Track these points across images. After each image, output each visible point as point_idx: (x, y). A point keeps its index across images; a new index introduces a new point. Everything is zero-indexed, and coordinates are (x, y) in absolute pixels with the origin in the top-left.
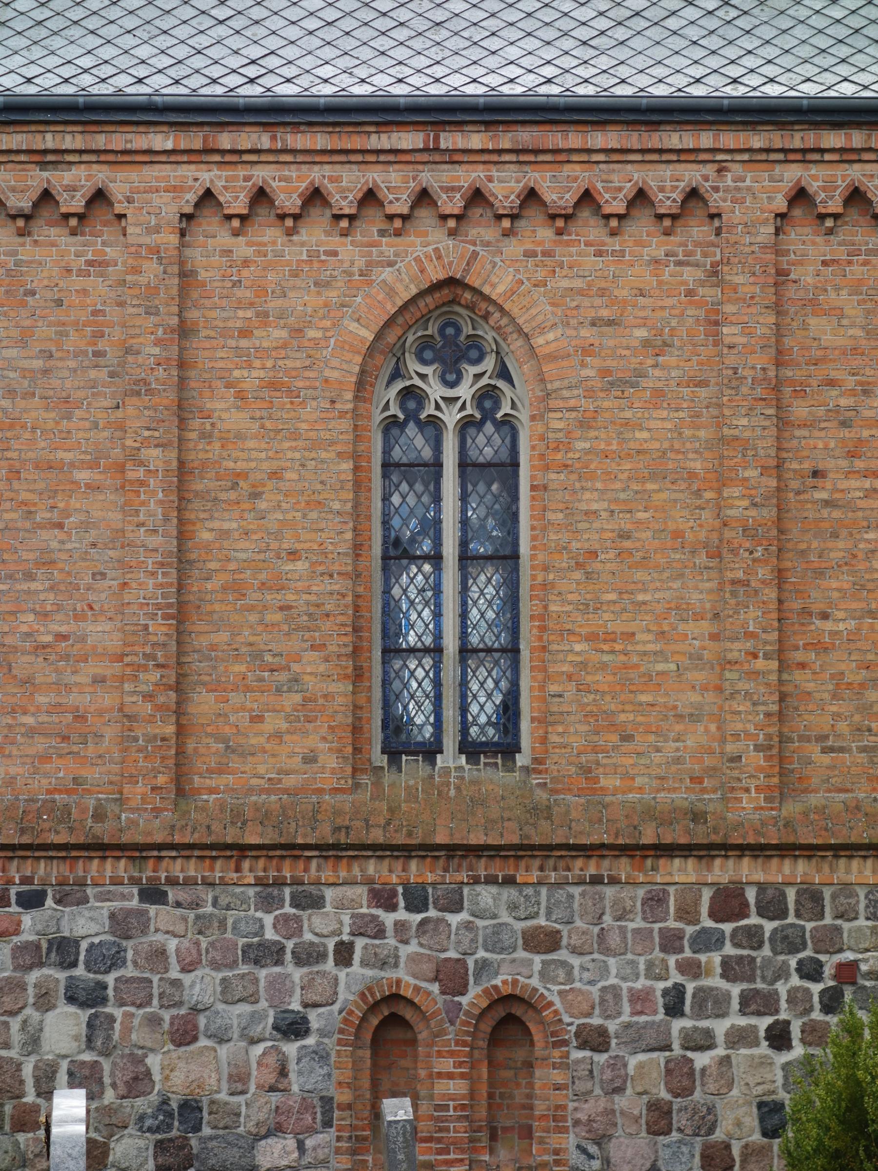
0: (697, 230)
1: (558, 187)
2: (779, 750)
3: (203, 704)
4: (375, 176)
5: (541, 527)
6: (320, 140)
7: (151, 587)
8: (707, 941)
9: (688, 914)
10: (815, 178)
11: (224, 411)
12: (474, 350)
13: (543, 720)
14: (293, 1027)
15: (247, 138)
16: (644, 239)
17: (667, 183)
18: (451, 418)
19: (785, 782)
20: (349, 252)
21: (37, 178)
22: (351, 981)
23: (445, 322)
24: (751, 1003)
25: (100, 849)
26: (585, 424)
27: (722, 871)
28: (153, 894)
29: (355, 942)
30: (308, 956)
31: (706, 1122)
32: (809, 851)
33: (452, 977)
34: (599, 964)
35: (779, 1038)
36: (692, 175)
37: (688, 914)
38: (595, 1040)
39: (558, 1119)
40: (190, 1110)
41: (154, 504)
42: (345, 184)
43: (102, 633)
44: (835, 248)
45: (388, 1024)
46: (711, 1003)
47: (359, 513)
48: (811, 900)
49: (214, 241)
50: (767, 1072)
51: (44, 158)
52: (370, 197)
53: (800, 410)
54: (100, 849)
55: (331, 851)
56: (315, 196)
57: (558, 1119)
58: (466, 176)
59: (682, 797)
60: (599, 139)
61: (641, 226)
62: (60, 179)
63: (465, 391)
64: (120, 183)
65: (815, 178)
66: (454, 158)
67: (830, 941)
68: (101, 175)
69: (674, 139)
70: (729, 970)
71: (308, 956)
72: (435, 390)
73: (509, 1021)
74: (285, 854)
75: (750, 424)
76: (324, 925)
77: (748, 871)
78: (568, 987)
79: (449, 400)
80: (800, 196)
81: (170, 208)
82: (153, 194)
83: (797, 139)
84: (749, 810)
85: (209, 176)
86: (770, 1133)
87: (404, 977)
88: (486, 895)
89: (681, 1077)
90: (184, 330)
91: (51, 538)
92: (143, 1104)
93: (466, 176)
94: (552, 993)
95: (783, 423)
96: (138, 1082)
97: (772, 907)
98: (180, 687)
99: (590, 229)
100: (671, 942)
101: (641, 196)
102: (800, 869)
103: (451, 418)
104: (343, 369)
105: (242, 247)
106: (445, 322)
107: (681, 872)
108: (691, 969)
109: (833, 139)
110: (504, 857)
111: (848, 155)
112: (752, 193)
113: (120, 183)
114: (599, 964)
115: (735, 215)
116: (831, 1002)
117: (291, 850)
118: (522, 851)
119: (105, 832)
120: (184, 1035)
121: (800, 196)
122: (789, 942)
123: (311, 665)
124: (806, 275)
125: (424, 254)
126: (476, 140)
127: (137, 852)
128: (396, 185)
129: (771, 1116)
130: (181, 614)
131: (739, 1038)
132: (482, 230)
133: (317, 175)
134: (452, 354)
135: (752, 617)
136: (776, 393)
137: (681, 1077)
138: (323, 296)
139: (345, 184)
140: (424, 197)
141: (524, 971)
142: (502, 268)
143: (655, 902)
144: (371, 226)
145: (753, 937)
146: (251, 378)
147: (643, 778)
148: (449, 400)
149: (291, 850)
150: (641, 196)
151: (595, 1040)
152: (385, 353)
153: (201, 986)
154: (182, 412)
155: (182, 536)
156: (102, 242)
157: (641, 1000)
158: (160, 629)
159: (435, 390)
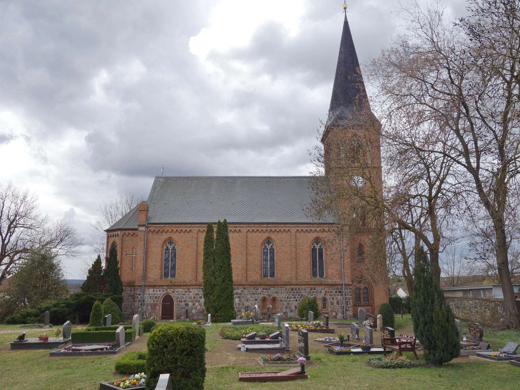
0: (289, 233)
1: (278, 229)
2: (296, 276)
3: (248, 272)
4: (263, 228)
5: (276, 258)
6: (258, 226)
7: (244, 263)
8: (290, 293)
9: (289, 290)
10: (299, 229)
11: (250, 248)
12: (271, 243)
13: (277, 274)
14: (256, 300)
15: (252, 225)
16: (285, 234)
17: (287, 229)
18: (170, 249)
19: (297, 279)
20: (260, 235)
21: (235, 229)
22: (261, 296)
23: (268, 241)
24: (294, 298)
25: (240, 285)
26: (280, 249)
27: (292, 287)
28: (245, 289)
29: (262, 293)
30: (257, 294)
31: (290, 308)
32: (299, 285)
33: (269, 296)
34: (282, 295)
35: (296, 301)
36: (289, 228)
37: (289, 290)
38: (281, 301)
39: (278, 308)
40: (248, 307)
41: (244, 256)
42: (260, 229)
43: (240, 267)
44: (300, 234)
45: (264, 300)
46: (291, 298)
47: (261, 257)
48: (299, 289)
49: (249, 234)
50: (295, 303)
51: (235, 227)
52: (262, 230)
53: (298, 248)
54: (240, 285)
55: (259, 285)
56: (258, 230)
57: (278, 308)
58: (270, 229)
59: (288, 280)
60: (281, 226)
61: (284, 232)
62: (237, 229)
63: (270, 246)
64: (241, 229)
65: (299, 229)
66: (269, 227)
67: (301, 292)
68: (240, 228)
69: (287, 225)
70: (292, 295)
71: (257, 294)
72: (169, 246)
73: (274, 299)
74: (255, 285)
75: (294, 249)
76: (259, 291)
77: (294, 287)
78: (279, 296)
79: (269, 247)
80: (298, 230)
81: (245, 231)
82: (244, 230)
83: (297, 225)
84: (294, 281)
85: (249, 229)
86: (296, 308)
87: (266, 296)
88: (272, 289)
89: (288, 304)
90: (247, 241)
91: (236, 259)
92: (244, 306)
93: (270, 229)
94: (278, 297)
95: (296, 249)
96: (243, 305)
97: (296, 290)
98: (247, 271)
99: (280, 233)
100: (287, 293)
101: (284, 230)
102: (298, 286)
103: (269, 248)
104: (309, 243)
105: (251, 234)
106: (268, 241)
107: (288, 287)
108: (289, 295)
109: (300, 225)
110: (274, 286)
111: (301, 227)
112: (294, 230)
113: (241, 229)
114: (282, 295)
115: (292, 232)
116: (301, 298)
117: (256, 285)
118: (275, 285)
119: (240, 284)
120: (247, 301)
121: (298, 230)
122: (297, 293)
123: (257, 270)
124: (298, 237)
125: (266, 235)
126: (271, 226)
127: (243, 285)
128: (264, 229)
129: (296, 307)
130: (247, 265)
131: (293, 301)
132: (271, 233)
133: (258, 228)
134: (269, 243)
135: (294, 265)
136: (296, 246)
137: (288, 304)
138: (259, 238)
139: (260, 229)
140: (262, 230)
141: (275, 295)
142: (273, 236)
143: (286, 289)
144: (262, 233)
145: (294, 292)
146: (252, 245)
147: (285, 278)
148: (170, 247)
149: (256, 285)
150: (284, 230)
151: (281, 301)
152: (165, 242)
153: (249, 296)
154: (247, 248)
155: (247, 258)
156: (240, 234)
157: (285, 297)
158: (245, 266)
159: (267, 246)
